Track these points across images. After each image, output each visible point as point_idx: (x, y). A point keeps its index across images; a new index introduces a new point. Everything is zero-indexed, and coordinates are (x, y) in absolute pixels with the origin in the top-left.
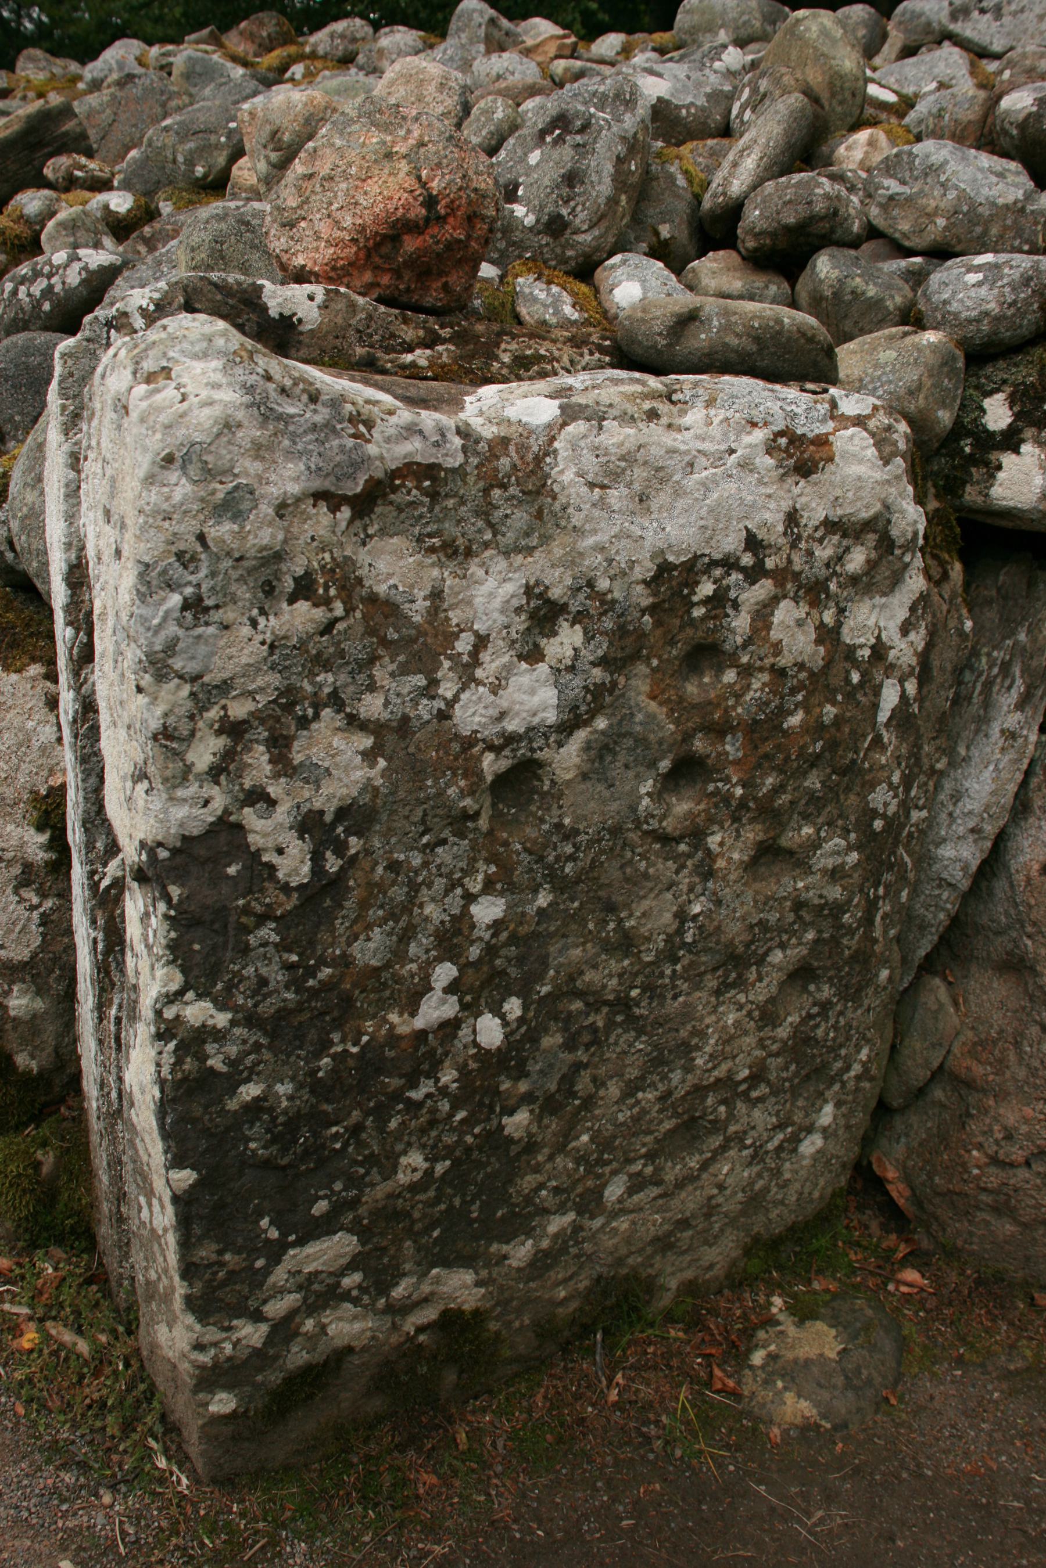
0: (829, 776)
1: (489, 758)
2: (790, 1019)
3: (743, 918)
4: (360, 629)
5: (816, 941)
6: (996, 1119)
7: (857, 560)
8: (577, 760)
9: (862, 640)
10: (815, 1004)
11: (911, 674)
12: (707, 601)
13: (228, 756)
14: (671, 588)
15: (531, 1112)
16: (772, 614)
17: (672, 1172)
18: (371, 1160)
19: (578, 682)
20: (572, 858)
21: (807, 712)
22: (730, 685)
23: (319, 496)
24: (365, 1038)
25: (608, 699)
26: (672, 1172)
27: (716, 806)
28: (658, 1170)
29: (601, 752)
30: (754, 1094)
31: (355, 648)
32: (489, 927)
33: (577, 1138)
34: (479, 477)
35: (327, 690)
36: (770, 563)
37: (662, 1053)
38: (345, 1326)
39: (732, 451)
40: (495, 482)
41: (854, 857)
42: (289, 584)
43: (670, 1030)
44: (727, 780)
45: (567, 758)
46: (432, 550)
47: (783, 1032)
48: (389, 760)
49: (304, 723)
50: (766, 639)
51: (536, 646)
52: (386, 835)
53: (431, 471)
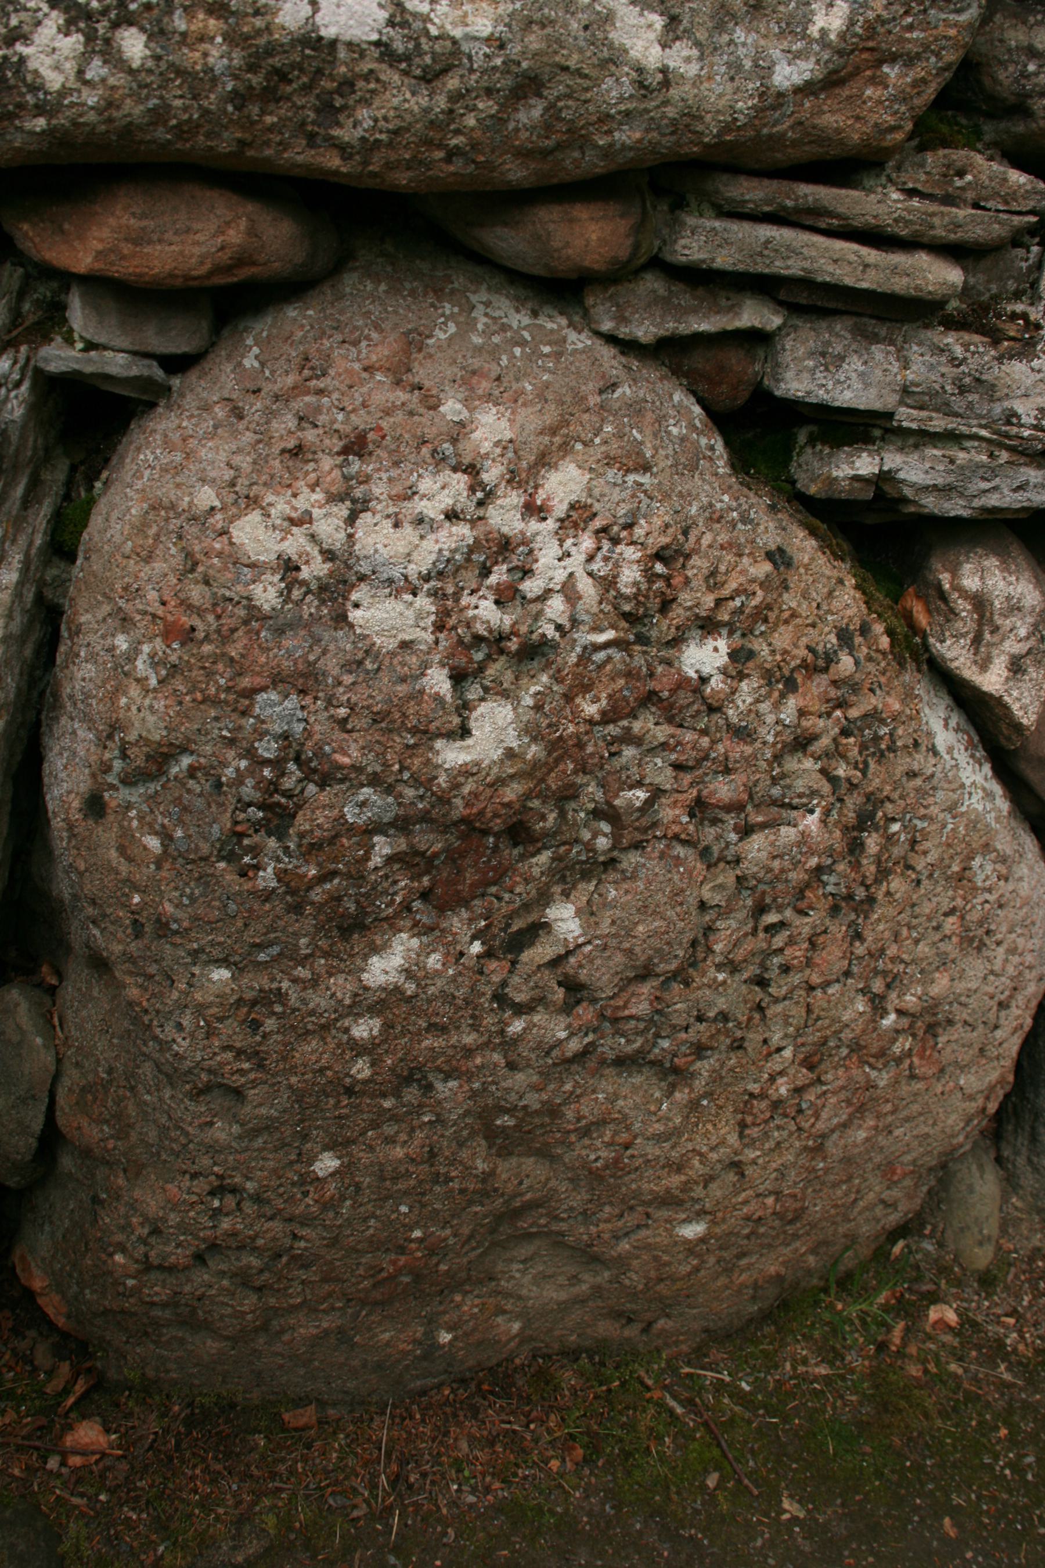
6: (133, 1206)
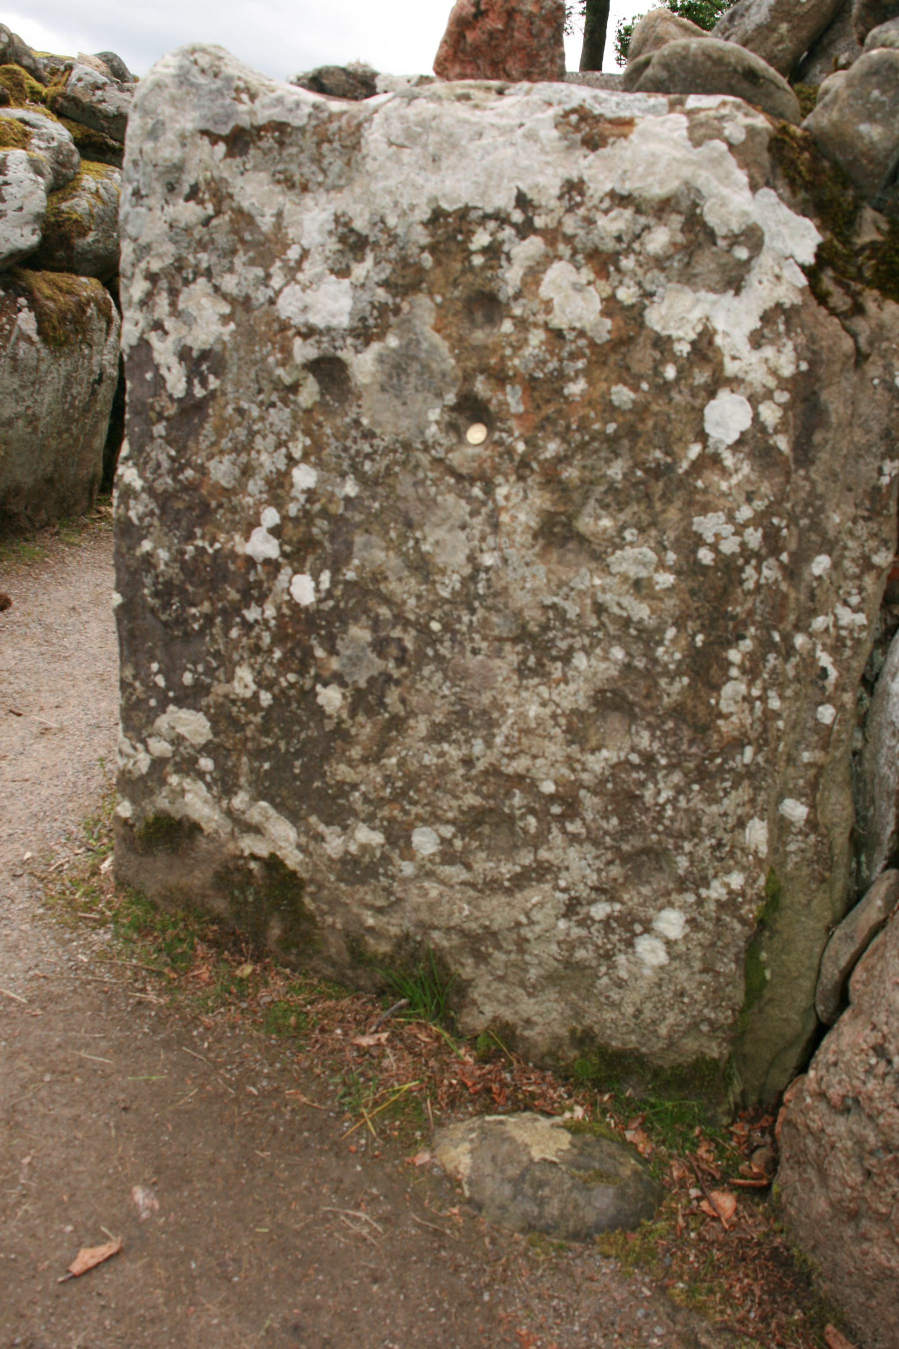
0: (632, 471)
1: (298, 341)
2: (605, 753)
3: (534, 592)
4: (227, 228)
5: (628, 668)
7: (659, 239)
8: (373, 369)
9: (681, 333)
10: (633, 749)
11: (769, 395)
12: (485, 251)
13: (149, 295)
14: (446, 232)
15: (344, 696)
16: (544, 271)
17: (483, 865)
18: (217, 654)
19: (366, 296)
20: (368, 456)
21: (591, 383)
22: (507, 335)
23: (204, 133)
24: (217, 545)
25: (392, 320)
26: (483, 865)
27: (501, 456)
28: (466, 849)
29: (397, 368)
30: (571, 827)
31: (222, 240)
32: (303, 492)
33: (389, 756)
34: (314, 134)
35: (204, 265)
36: (539, 222)
37: (466, 710)
38: (197, 803)
39: (522, 125)
40: (324, 139)
41: (666, 579)
42: (186, 189)
43: (472, 689)
44: (510, 432)
45: (364, 365)
46: (279, 182)
47: (597, 763)
48: (238, 325)
49: (186, 282)
50: (535, 294)
51: (348, 267)
52: (237, 384)
53: (280, 127)
